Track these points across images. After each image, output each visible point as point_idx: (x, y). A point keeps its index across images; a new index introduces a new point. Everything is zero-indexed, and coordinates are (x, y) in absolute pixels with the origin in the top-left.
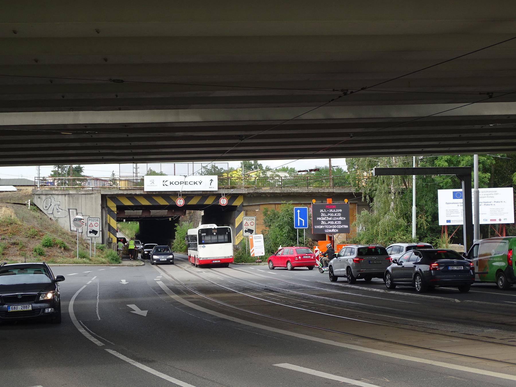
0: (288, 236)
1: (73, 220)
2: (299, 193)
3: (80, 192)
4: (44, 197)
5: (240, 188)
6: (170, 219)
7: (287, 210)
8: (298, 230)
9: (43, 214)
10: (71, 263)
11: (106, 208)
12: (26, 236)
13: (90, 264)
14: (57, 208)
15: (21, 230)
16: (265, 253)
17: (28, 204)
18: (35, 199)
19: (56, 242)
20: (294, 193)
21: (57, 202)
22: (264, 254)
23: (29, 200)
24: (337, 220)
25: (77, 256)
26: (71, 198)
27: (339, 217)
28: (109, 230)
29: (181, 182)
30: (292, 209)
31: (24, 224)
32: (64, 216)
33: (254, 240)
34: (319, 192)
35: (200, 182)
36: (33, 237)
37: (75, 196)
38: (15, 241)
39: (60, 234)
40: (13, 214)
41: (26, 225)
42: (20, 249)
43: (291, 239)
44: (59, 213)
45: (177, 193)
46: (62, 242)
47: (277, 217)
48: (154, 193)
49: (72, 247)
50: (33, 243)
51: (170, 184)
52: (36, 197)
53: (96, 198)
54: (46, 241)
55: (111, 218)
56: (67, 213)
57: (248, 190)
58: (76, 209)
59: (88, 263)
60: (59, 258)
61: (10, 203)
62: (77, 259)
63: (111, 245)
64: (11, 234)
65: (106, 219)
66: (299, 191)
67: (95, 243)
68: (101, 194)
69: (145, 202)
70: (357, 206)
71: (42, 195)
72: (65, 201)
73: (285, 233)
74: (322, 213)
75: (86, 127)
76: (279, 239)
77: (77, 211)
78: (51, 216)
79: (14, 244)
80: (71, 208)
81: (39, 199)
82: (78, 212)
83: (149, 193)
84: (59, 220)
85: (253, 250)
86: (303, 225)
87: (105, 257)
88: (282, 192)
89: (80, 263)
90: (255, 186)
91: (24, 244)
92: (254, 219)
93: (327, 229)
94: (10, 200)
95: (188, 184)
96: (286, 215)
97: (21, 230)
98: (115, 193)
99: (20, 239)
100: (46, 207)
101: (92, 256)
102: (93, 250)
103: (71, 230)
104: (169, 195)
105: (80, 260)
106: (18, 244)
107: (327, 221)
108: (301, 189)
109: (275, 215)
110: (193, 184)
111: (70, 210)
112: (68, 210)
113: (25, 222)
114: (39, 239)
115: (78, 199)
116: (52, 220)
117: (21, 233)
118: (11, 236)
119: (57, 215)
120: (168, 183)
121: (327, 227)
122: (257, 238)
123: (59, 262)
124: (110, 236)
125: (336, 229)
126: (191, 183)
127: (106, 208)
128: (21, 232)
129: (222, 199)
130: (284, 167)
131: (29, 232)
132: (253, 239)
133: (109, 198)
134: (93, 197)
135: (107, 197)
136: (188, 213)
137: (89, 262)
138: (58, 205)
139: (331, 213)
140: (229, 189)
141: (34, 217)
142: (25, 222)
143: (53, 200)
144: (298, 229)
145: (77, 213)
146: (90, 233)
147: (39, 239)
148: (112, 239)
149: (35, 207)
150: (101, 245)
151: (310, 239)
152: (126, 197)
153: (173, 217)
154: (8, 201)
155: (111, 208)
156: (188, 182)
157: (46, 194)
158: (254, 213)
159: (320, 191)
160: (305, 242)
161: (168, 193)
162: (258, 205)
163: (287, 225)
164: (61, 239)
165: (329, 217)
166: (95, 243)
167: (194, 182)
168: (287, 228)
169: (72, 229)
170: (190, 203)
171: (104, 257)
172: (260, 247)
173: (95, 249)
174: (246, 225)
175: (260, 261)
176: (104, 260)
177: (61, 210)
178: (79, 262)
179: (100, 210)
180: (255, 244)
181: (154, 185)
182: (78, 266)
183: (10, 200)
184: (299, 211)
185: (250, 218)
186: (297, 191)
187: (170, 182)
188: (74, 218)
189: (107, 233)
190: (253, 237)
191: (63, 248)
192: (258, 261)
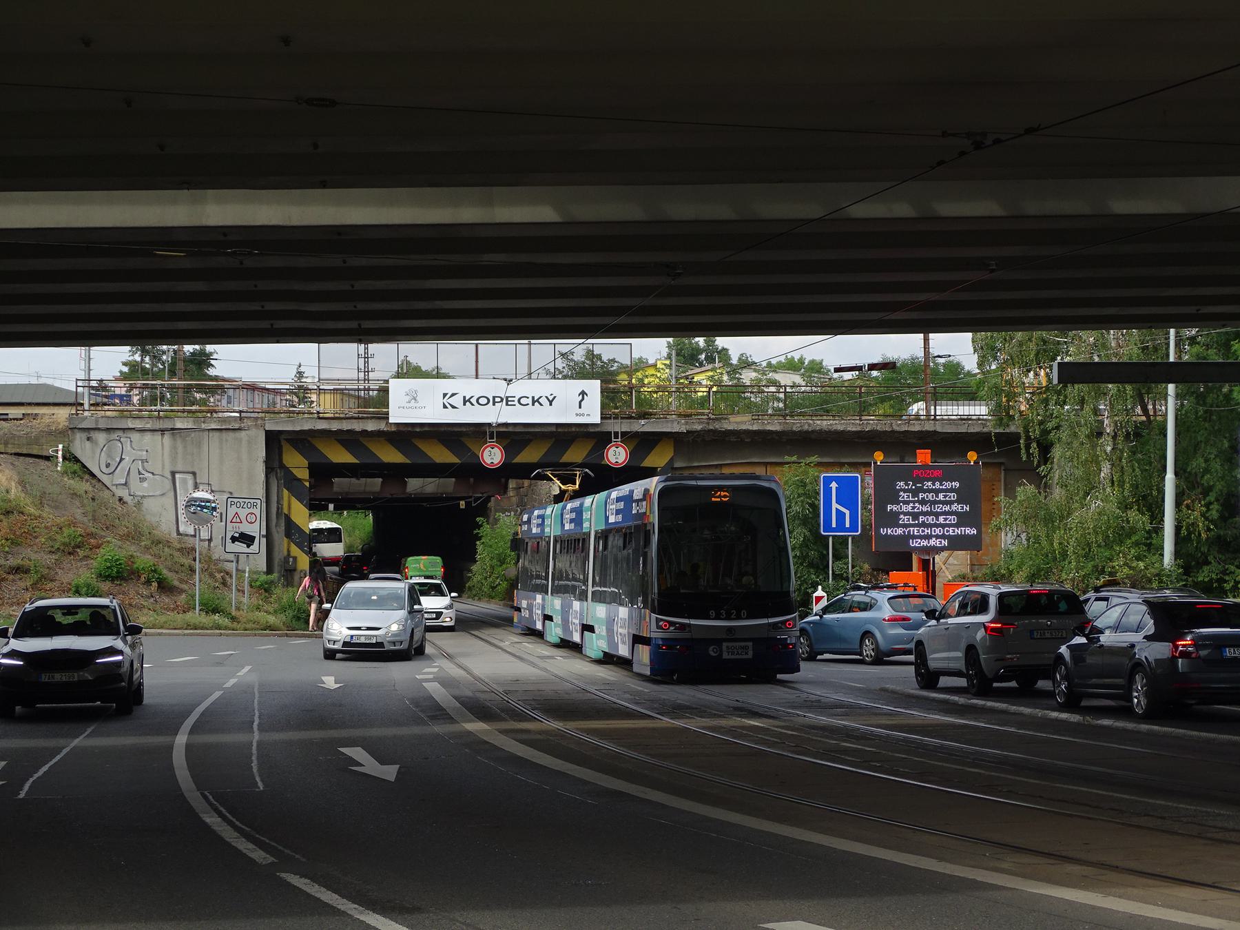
1: (184, 503)
2: (837, 432)
4: (101, 438)
6: (462, 504)
8: (831, 539)
9: (98, 485)
10: (178, 627)
11: (279, 471)
12: (49, 549)
13: (233, 630)
15: (35, 532)
17: (57, 457)
19: (135, 566)
20: (821, 432)
21: (140, 453)
23: (61, 446)
24: (945, 513)
25: (195, 609)
27: (951, 503)
28: (288, 535)
29: (494, 398)
30: (816, 480)
32: (158, 493)
35: (551, 398)
36: (71, 550)
38: (19, 561)
39: (148, 543)
40: (13, 484)
43: (811, 565)
44: (145, 484)
45: (483, 428)
46: (154, 565)
48: (418, 430)
49: (181, 581)
51: (464, 404)
52: (79, 436)
54: (108, 564)
55: (293, 499)
56: (168, 484)
57: (686, 423)
58: (194, 474)
59: (226, 628)
60: (145, 611)
61: (6, 453)
62: (196, 616)
63: (293, 578)
64: (9, 543)
65: (278, 502)
66: (835, 428)
67: (247, 570)
69: (390, 455)
70: (1003, 472)
71: (96, 432)
72: (163, 449)
75: (225, 235)
77: (195, 478)
79: (16, 571)
80: (179, 467)
81: (87, 442)
82: (198, 481)
83: (402, 429)
84: (147, 503)
86: (847, 525)
87: (275, 611)
88: (787, 428)
90: (709, 413)
91: (46, 571)
93: (914, 537)
95: (516, 403)
96: (799, 496)
97: (35, 532)
98: (306, 427)
100: (108, 466)
101: (238, 609)
103: (179, 533)
104: (461, 434)
105: (204, 619)
106: (27, 571)
107: (915, 516)
108: (843, 422)
110: (531, 403)
111: (177, 476)
112: (170, 477)
113: (47, 509)
114: (86, 557)
115: (199, 445)
116: (124, 503)
117: (38, 540)
118: (7, 549)
119: (139, 488)
121: (915, 531)
124: (289, 551)
125: (943, 537)
126: (523, 401)
127: (279, 471)
128: (36, 537)
129: (614, 448)
130: (793, 358)
131: (58, 537)
133: (288, 440)
134: (240, 440)
136: (514, 486)
137: (230, 624)
138: (142, 460)
139: (929, 491)
140: (634, 418)
141: (75, 494)
142: (47, 509)
143: (128, 447)
144: (833, 536)
145: (196, 483)
146: (233, 542)
147: (86, 557)
148: (295, 558)
149: (76, 467)
150: (263, 578)
151: (866, 566)
152: (336, 440)
153: (471, 497)
155: (295, 471)
156: (516, 399)
157: (108, 430)
159: (896, 428)
160: (853, 574)
164: (150, 557)
165: (923, 502)
166: (247, 570)
167: (533, 398)
169: (182, 529)
171: (271, 610)
173: (247, 588)
176: (272, 619)
177: (150, 475)
178: (201, 625)
181: (417, 405)
183: (6, 444)
184: (834, 485)
187: (464, 397)
188: (187, 499)
189: (282, 544)
191: (155, 584)
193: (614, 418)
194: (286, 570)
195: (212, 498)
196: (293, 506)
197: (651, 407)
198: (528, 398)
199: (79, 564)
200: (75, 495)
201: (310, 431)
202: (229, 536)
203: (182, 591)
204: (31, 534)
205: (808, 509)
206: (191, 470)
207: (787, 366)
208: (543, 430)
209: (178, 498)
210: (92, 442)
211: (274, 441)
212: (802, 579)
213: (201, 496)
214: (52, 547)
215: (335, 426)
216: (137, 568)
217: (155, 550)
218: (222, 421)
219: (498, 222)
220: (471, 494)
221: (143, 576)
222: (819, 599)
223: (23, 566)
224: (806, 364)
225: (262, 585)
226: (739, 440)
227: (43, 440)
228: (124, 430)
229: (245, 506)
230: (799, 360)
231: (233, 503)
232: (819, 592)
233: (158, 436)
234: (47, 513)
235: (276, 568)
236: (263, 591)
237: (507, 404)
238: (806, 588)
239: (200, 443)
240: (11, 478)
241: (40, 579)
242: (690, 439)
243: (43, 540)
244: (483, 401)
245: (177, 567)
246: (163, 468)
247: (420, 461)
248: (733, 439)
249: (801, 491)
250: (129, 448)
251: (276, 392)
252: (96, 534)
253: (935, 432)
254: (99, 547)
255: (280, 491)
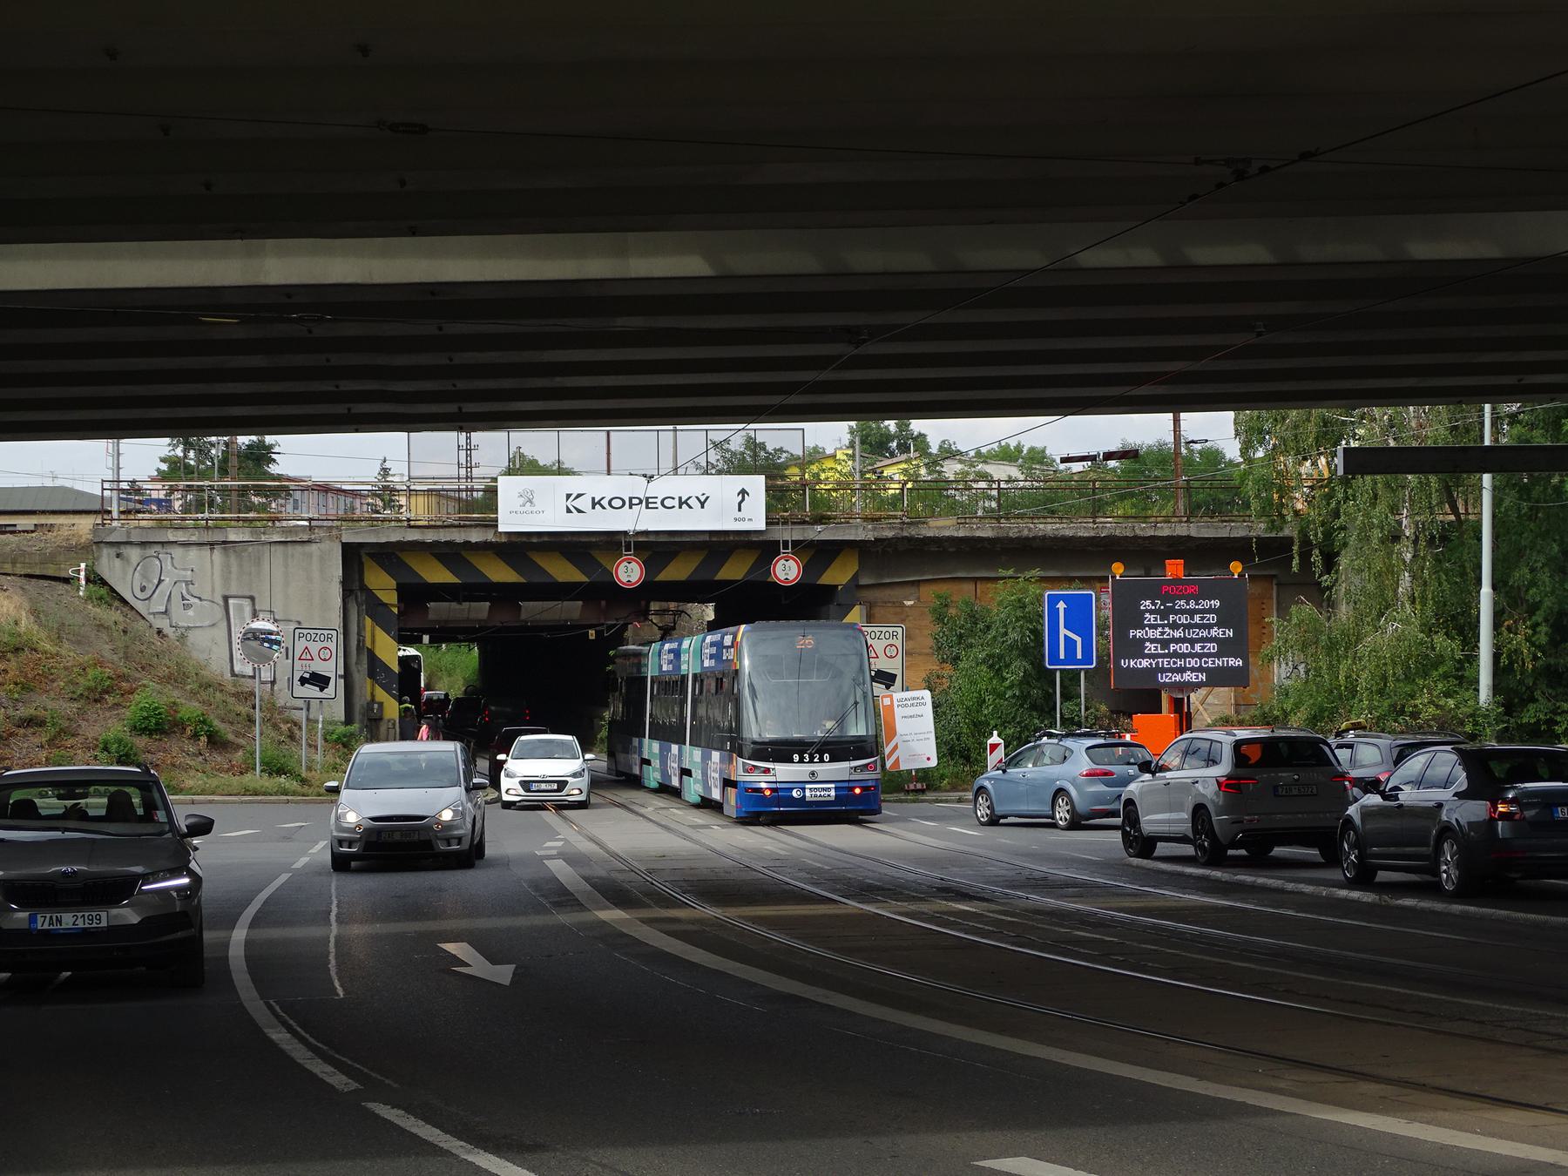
0: (1024, 697)
1: (241, 636)
2: (1065, 539)
3: (264, 533)
4: (134, 554)
5: (848, 523)
6: (592, 634)
7: (1019, 600)
8: (1058, 674)
9: (131, 614)
13: (303, 795)
14: (184, 592)
16: (939, 759)
17: (79, 579)
18: (104, 561)
19: (179, 715)
20: (1044, 538)
21: (183, 573)
22: (934, 763)
23: (83, 565)
24: (1203, 640)
25: (254, 769)
26: (233, 560)
28: (372, 674)
29: (631, 499)
30: (1039, 599)
31: (63, 652)
32: (207, 623)
33: (898, 712)
34: (1136, 537)
35: (702, 499)
36: (97, 696)
37: (246, 550)
38: (32, 711)
39: (195, 686)
40: (24, 614)
41: (69, 653)
42: (51, 742)
43: (1034, 707)
44: (191, 613)
47: (981, 625)
49: (237, 734)
50: (96, 721)
51: (593, 508)
53: (322, 559)
54: (145, 714)
56: (220, 612)
57: (874, 529)
58: (252, 599)
59: (294, 793)
60: (192, 773)
61: (14, 575)
62: (256, 778)
64: (18, 688)
66: (1062, 533)
67: (321, 719)
68: (342, 543)
69: (500, 573)
70: (1275, 587)
71: (128, 547)
73: (1011, 687)
74: (1147, 611)
75: (289, 296)
76: (991, 708)
77: (254, 604)
78: (161, 623)
79: (28, 725)
80: (233, 592)
83: (514, 539)
84: (193, 637)
85: (896, 747)
86: (1079, 656)
88: (1002, 534)
89: (264, 794)
90: (903, 515)
92: (900, 636)
93: (1164, 670)
94: (14, 563)
95: (659, 505)
99: (50, 704)
100: (143, 589)
101: (309, 769)
102: (312, 746)
103: (233, 674)
104: (589, 545)
105: (267, 782)
106: (42, 724)
107: (1165, 643)
109: (973, 618)
110: (677, 506)
111: (231, 601)
112: (221, 603)
113: (66, 645)
115: (258, 562)
116: (165, 636)
117: (55, 685)
118: (16, 696)
119: (183, 618)
120: (584, 503)
121: (1165, 663)
122: (909, 703)
123: (191, 788)
124: (373, 695)
125: (1200, 669)
126: (667, 503)
128: (53, 681)
129: (782, 561)
131: (81, 680)
132: (895, 706)
133: (371, 556)
134: (310, 556)
135: (363, 552)
137: (299, 789)
138: (187, 583)
139: (1182, 612)
141: (102, 625)
142: (66, 645)
143: (168, 566)
144: (1060, 669)
146: (302, 685)
147: (117, 705)
148: (381, 705)
149: (103, 591)
150: (341, 729)
151: (1103, 708)
152: (431, 554)
154: (6, 566)
155: (379, 594)
156: (659, 501)
157: (143, 544)
158: (896, 614)
159: (1139, 533)
160: (1086, 718)
161: (583, 540)
162: (913, 583)
163: (1019, 656)
164: (197, 704)
165: (1174, 626)
166: (321, 719)
167: (680, 498)
168: (1017, 670)
169: (237, 669)
170: (662, 577)
172: (921, 737)
173: (320, 742)
174: (303, 657)
175: (919, 786)
177: (197, 600)
178: (263, 789)
179: (338, 601)
180: (901, 726)
181: (534, 509)
182: (260, 802)
183: (14, 563)
184: (1061, 606)
185: (884, 629)
186: (1056, 533)
187: (593, 499)
188: (243, 631)
189: (364, 686)
190: (895, 701)
191: (204, 739)
192: (912, 787)
193: (783, 524)
194: (370, 720)
195: (276, 629)
196: (378, 638)
197: (830, 509)
198: (673, 498)
199: (108, 714)
200: (101, 627)
201: (399, 542)
202: (297, 677)
203: (239, 747)
204: (47, 677)
205: (1029, 636)
206: (248, 594)
207: (1001, 455)
208: (693, 539)
209: (233, 629)
210: (122, 559)
211: (353, 555)
212: (1023, 725)
213: (260, 627)
214: (74, 692)
215: (430, 537)
216: (181, 718)
217: (204, 695)
218: (287, 532)
219: (633, 276)
220: (602, 621)
221: (188, 729)
222: (994, 747)
223: (36, 717)
224: (1025, 452)
225: (339, 738)
226: (941, 549)
227: (62, 558)
228: (162, 543)
229: (317, 639)
230: (1015, 448)
231: (301, 635)
232: (995, 739)
233: (206, 551)
234: (66, 649)
235: (357, 716)
236: (340, 745)
237: (647, 507)
238: (1028, 736)
239: (259, 559)
240: (20, 607)
241: (59, 733)
242: (880, 549)
243: (62, 684)
244: (617, 503)
245: (232, 716)
246: (213, 590)
247: (537, 579)
248: (934, 548)
249: (1019, 613)
250: (170, 567)
251: (354, 494)
252: (129, 676)
253: (1189, 537)
254: (132, 693)
255: (362, 619)
